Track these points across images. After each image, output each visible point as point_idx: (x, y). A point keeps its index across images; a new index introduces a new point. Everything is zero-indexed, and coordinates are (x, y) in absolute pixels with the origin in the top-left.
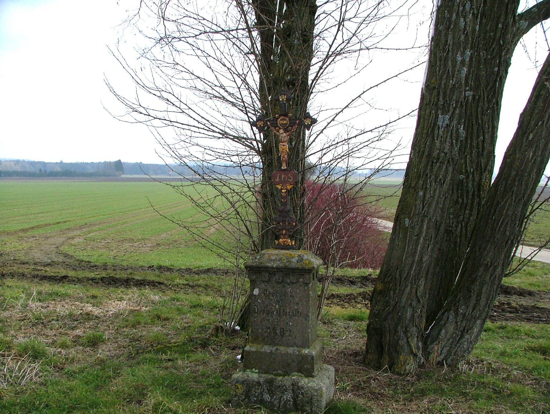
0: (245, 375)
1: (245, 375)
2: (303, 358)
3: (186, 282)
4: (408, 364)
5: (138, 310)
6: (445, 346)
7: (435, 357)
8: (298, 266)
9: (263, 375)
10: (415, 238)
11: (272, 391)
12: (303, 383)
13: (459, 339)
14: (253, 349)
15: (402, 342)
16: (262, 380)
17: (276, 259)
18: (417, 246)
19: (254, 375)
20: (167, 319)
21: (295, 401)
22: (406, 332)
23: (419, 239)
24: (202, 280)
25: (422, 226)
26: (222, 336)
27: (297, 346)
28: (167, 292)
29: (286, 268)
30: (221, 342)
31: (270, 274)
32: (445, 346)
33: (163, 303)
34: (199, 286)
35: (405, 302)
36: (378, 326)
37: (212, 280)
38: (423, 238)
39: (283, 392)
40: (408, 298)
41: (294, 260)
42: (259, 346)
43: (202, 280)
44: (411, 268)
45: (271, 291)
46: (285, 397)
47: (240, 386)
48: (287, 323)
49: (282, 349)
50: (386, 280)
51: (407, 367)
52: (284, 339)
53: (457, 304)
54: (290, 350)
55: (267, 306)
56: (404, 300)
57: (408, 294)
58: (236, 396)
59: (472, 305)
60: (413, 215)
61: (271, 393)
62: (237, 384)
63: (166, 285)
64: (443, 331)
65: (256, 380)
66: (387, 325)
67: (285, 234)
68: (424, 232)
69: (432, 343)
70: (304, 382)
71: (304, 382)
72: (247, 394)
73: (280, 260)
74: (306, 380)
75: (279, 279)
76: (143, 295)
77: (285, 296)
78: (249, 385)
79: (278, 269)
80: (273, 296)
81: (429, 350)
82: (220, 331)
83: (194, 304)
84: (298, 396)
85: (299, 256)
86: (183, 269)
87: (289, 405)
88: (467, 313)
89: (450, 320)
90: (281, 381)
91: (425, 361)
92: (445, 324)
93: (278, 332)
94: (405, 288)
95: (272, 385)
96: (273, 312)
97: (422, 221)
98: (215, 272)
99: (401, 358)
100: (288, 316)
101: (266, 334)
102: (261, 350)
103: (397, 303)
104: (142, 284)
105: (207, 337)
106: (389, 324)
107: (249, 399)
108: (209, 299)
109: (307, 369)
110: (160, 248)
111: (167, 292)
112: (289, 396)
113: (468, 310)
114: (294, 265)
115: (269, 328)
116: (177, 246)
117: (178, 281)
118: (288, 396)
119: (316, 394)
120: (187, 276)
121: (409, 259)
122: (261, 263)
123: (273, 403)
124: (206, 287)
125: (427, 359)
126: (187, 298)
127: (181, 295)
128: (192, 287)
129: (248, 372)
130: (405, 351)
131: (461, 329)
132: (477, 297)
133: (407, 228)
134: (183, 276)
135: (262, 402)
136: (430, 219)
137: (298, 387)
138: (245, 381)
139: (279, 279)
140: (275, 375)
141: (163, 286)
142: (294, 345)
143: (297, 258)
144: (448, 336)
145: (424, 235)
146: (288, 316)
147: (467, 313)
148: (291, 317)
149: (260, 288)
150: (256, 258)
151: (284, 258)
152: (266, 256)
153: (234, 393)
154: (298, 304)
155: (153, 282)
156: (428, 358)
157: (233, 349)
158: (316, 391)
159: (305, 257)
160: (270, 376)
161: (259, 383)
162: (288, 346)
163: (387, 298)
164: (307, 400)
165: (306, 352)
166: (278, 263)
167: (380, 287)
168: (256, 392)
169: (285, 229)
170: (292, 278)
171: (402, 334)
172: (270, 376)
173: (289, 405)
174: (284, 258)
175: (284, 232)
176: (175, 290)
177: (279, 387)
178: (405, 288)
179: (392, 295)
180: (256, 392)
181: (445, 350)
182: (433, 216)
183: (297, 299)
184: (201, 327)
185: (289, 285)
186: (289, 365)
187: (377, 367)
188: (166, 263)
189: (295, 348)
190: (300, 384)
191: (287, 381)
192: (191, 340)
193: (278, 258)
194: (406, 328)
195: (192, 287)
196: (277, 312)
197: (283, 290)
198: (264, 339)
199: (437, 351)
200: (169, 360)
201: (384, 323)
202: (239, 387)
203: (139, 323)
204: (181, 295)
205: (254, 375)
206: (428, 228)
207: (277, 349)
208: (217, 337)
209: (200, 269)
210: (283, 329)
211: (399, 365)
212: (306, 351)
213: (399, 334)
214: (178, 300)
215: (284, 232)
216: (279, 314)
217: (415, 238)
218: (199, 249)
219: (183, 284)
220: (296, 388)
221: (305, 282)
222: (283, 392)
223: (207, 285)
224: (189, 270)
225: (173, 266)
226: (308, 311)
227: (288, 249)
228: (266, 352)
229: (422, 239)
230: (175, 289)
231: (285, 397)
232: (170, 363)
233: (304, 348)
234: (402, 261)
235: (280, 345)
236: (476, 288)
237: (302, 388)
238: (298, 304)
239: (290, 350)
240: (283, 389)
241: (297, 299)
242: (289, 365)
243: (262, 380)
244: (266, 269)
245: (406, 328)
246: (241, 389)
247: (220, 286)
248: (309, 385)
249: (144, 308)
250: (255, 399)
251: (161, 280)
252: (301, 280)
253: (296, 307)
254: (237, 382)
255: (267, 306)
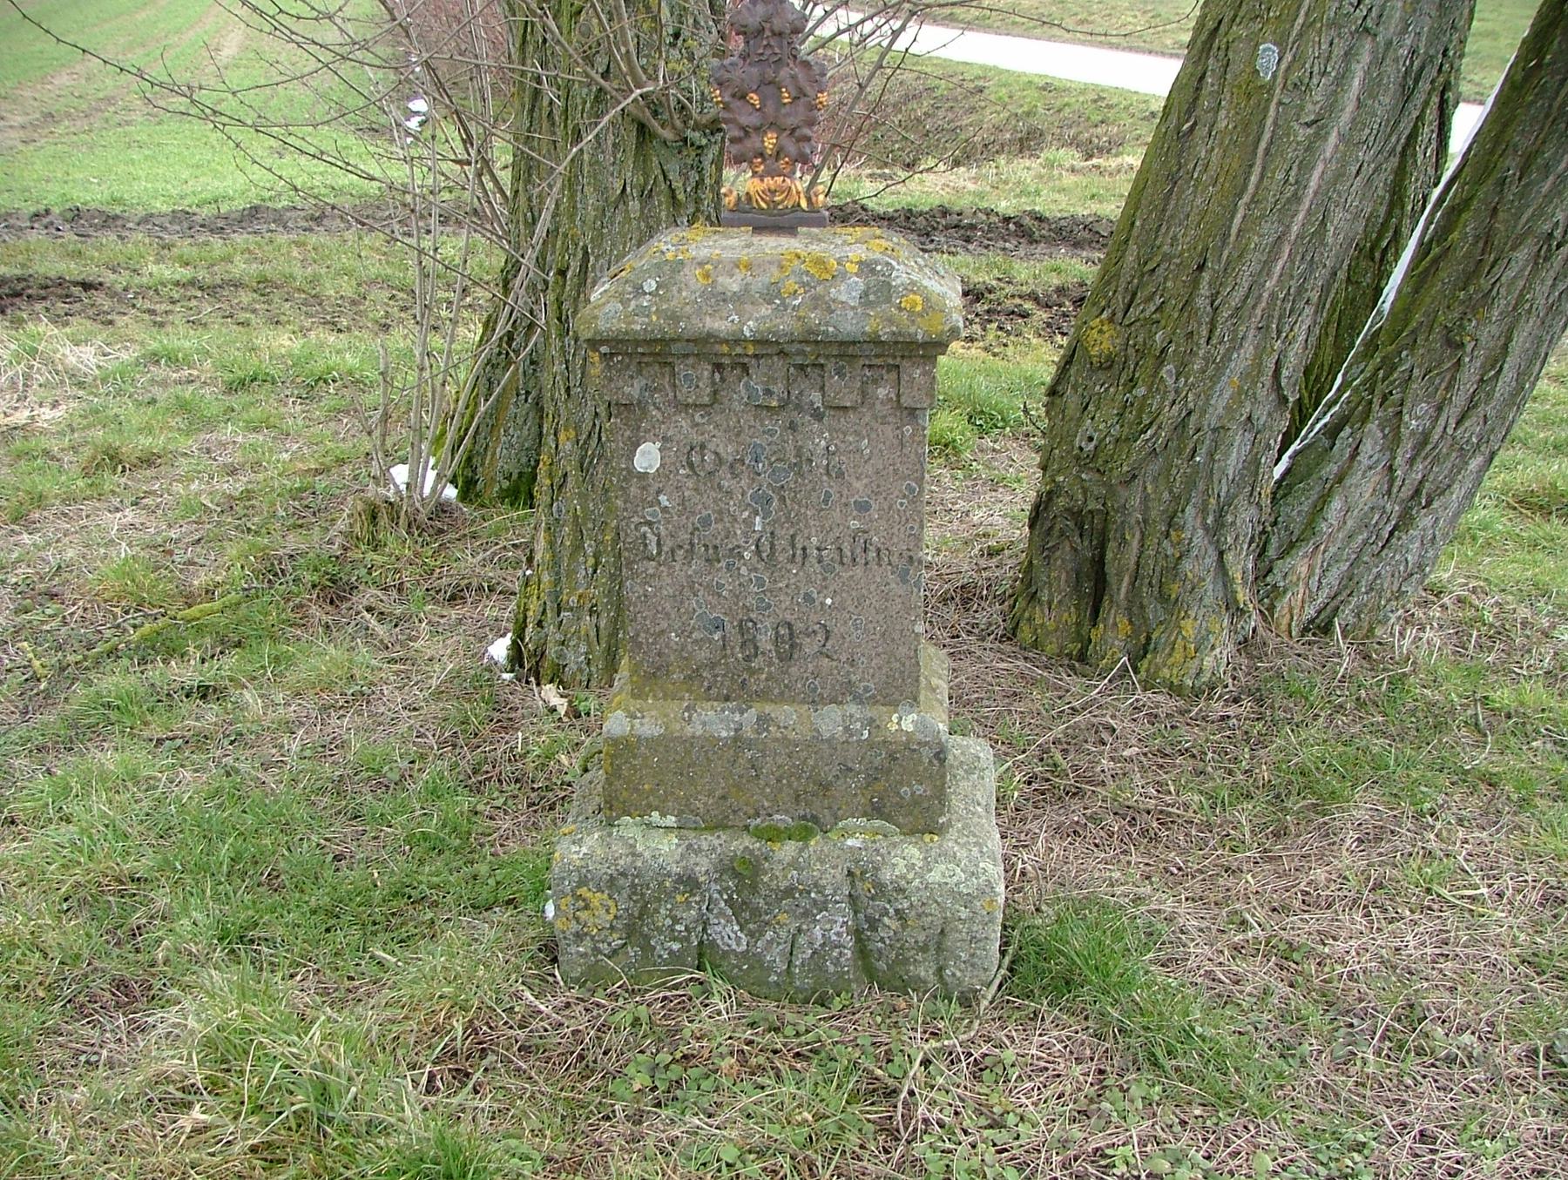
0: (618, 849)
1: (618, 849)
2: (892, 758)
3: (184, 273)
4: (1213, 648)
5: (23, 428)
6: (1336, 559)
7: (1297, 605)
8: (874, 324)
9: (707, 840)
10: (1303, 133)
11: (756, 912)
12: (901, 869)
13: (1391, 533)
14: (649, 728)
15: (1198, 566)
16: (702, 866)
17: (746, 288)
18: (1306, 167)
19: (658, 845)
20: (148, 460)
21: (862, 951)
22: (1215, 531)
23: (1320, 136)
24: (240, 257)
25: (1342, 80)
26: (396, 542)
27: (859, 700)
28: (121, 321)
29: (810, 339)
30: (397, 571)
31: (718, 367)
32: (1336, 559)
33: (116, 382)
34: (237, 285)
35: (1227, 408)
36: (1092, 505)
37: (285, 255)
38: (1341, 136)
39: (806, 914)
40: (1240, 394)
41: (848, 292)
42: (674, 708)
43: (240, 257)
44: (1267, 266)
45: (728, 451)
46: (818, 931)
47: (596, 899)
48: (808, 598)
49: (787, 714)
50: (1133, 313)
51: (1208, 662)
52: (793, 670)
53: (1396, 397)
54: (831, 721)
55: (706, 522)
56: (1219, 403)
57: (1244, 376)
58: (579, 937)
59: (1459, 400)
60: (1307, 26)
61: (742, 910)
62: (583, 891)
63: (112, 294)
64: (1336, 504)
65: (676, 869)
66: (1136, 501)
67: (778, 155)
68: (1350, 107)
69: (1288, 549)
70: (904, 859)
71: (904, 859)
72: (635, 929)
73: (771, 294)
74: (914, 852)
75: (768, 392)
76: (33, 352)
77: (800, 474)
78: (640, 895)
79: (770, 347)
80: (735, 476)
81: (1275, 578)
82: (384, 520)
83: (241, 374)
84: (874, 924)
85: (866, 267)
86: (161, 215)
87: (836, 963)
88: (1439, 429)
89: (1363, 458)
90: (794, 864)
91: (1261, 624)
92: (1340, 479)
93: (765, 641)
94: (1229, 351)
95: (754, 889)
96: (736, 553)
97: (1349, 55)
98: (279, 219)
99: (1189, 628)
100: (813, 567)
101: (703, 655)
102: (689, 730)
103: (1189, 414)
104: (18, 295)
105: (336, 549)
106: (1146, 499)
107: (647, 948)
108: (285, 342)
109: (916, 801)
110: (60, 130)
111: (121, 321)
112: (837, 928)
113: (1442, 422)
114: (849, 324)
115: (718, 626)
116: (117, 119)
117: (157, 270)
118: (835, 926)
119: (964, 913)
120: (184, 247)
121: (1266, 227)
122: (674, 318)
123: (759, 958)
124: (264, 286)
125: (1268, 613)
126: (208, 344)
127: (181, 339)
128: (212, 290)
129: (629, 827)
130: (1206, 601)
131: (1406, 492)
132: (1484, 369)
133: (1270, 89)
134: (168, 247)
135: (705, 955)
136: (1389, 44)
137: (880, 886)
138: (623, 874)
139: (768, 392)
140: (759, 834)
141: (100, 298)
142: (846, 692)
143: (859, 283)
144: (1350, 523)
145: (1346, 117)
146: (813, 567)
147: (1439, 429)
148: (828, 569)
149: (665, 439)
150: (639, 291)
151: (791, 284)
152: (694, 279)
153: (574, 926)
154: (863, 507)
155: (60, 282)
156: (1271, 608)
157: (454, 598)
158: (968, 900)
159: (900, 276)
160: (743, 843)
161: (689, 882)
162: (815, 701)
163: (1141, 391)
164: (922, 938)
165: (908, 725)
166: (765, 310)
167: (1103, 340)
168: (676, 920)
169: (773, 125)
170: (842, 388)
171: (1200, 538)
172: (743, 843)
173: (836, 963)
174: (791, 284)
175: (770, 141)
176: (152, 312)
177: (789, 892)
178: (1229, 351)
179: (1170, 381)
180: (676, 920)
181: (1333, 577)
182: (1404, 31)
183: (857, 485)
184: (295, 495)
185: (818, 416)
186: (825, 787)
187: (1070, 656)
188: (93, 195)
189: (853, 709)
190: (886, 875)
191: (823, 860)
192: (271, 572)
193: (759, 283)
194: (1220, 515)
195: (212, 290)
196: (758, 552)
197: (790, 447)
198: (694, 676)
199: (1305, 580)
200: (204, 692)
201: (1123, 493)
202: (595, 903)
203: (40, 500)
204: (181, 339)
205: (658, 845)
206: (1371, 87)
207: (763, 721)
208: (376, 546)
209: (224, 209)
210: (790, 626)
211: (1178, 656)
212: (906, 722)
213: (1186, 535)
214: (173, 360)
215: (770, 141)
216: (767, 556)
217: (1303, 133)
218: (197, 125)
219: (177, 284)
220: (867, 892)
221: (906, 401)
222: (806, 914)
223: (263, 280)
224: (184, 220)
225: (116, 200)
226: (918, 538)
227: (791, 230)
228: (714, 740)
229: (1333, 139)
230: (147, 305)
231: (818, 931)
232: (212, 714)
233: (894, 704)
234: (1226, 236)
235: (781, 699)
236: (1487, 332)
237: (901, 890)
238: (863, 507)
239: (831, 721)
240: (804, 900)
241: (857, 485)
242: (825, 787)
243: (702, 866)
244: (702, 346)
245: (1220, 515)
246: (603, 911)
247: (314, 280)
248: (934, 876)
249: (47, 413)
250: (676, 946)
251: (91, 272)
252: (882, 392)
253: (854, 524)
254: (583, 882)
255: (706, 522)
